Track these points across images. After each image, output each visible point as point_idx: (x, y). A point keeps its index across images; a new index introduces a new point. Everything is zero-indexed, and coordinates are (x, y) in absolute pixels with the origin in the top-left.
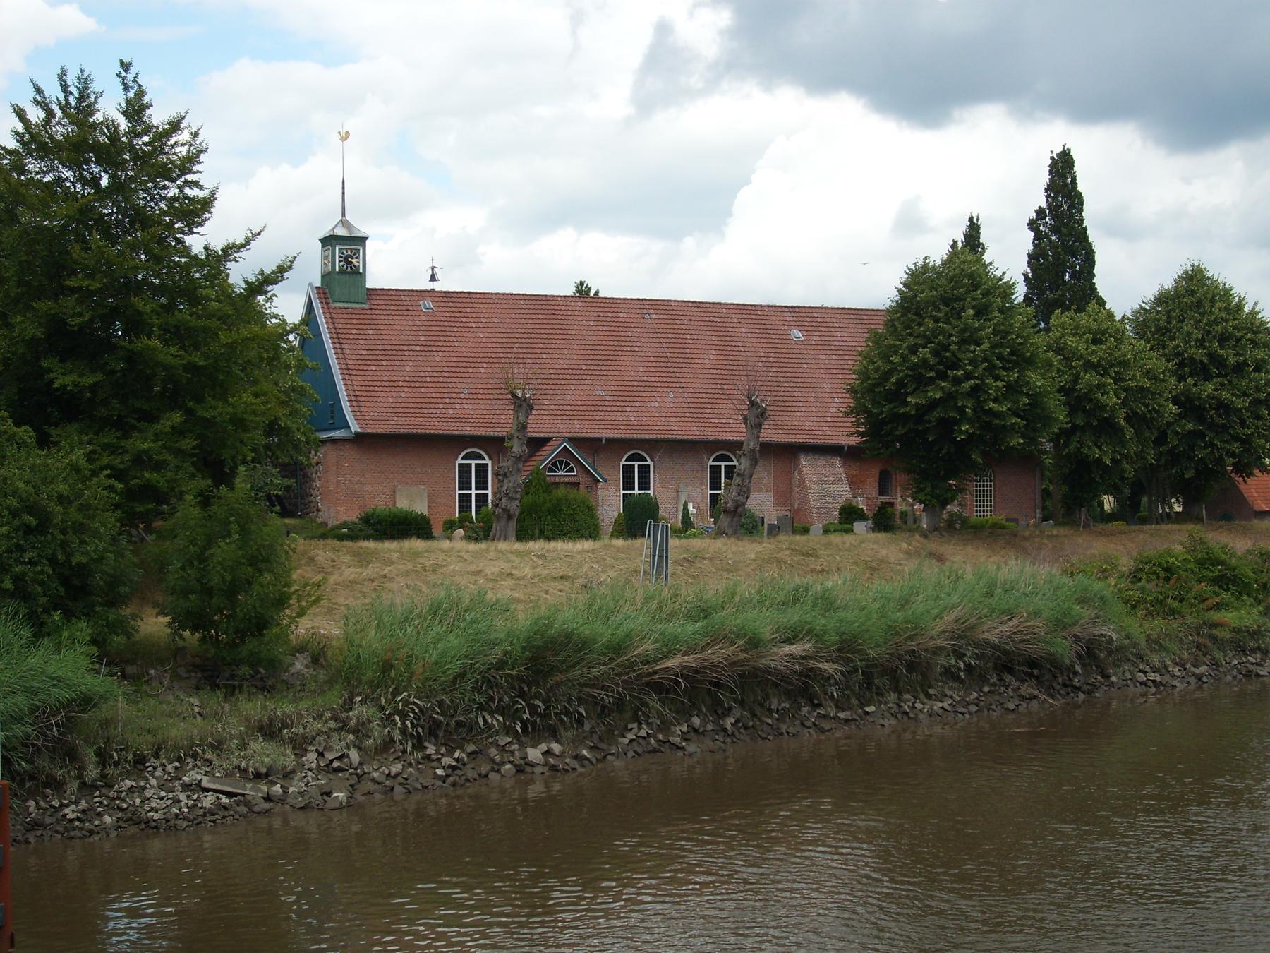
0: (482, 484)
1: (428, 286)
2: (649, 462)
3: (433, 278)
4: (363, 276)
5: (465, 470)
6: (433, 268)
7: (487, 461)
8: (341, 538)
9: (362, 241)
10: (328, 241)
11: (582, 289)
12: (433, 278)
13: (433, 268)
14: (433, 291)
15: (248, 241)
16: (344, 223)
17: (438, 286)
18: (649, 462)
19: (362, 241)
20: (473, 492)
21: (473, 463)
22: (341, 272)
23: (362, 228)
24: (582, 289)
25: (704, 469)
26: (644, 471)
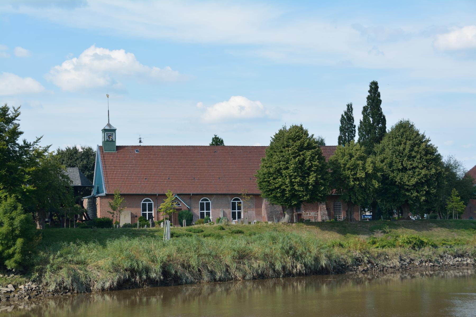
0: (150, 209)
1: (139, 144)
2: (210, 201)
3: (140, 142)
4: (115, 142)
5: (234, 204)
6: (140, 138)
7: (152, 202)
8: (235, 233)
9: (114, 130)
10: (105, 130)
11: (217, 142)
12: (140, 142)
13: (140, 138)
14: (140, 146)
15: (41, 137)
16: (109, 125)
17: (142, 144)
18: (210, 201)
19: (114, 130)
20: (147, 212)
21: (205, 202)
22: (107, 141)
23: (114, 126)
24: (217, 142)
25: (229, 203)
26: (208, 205)
